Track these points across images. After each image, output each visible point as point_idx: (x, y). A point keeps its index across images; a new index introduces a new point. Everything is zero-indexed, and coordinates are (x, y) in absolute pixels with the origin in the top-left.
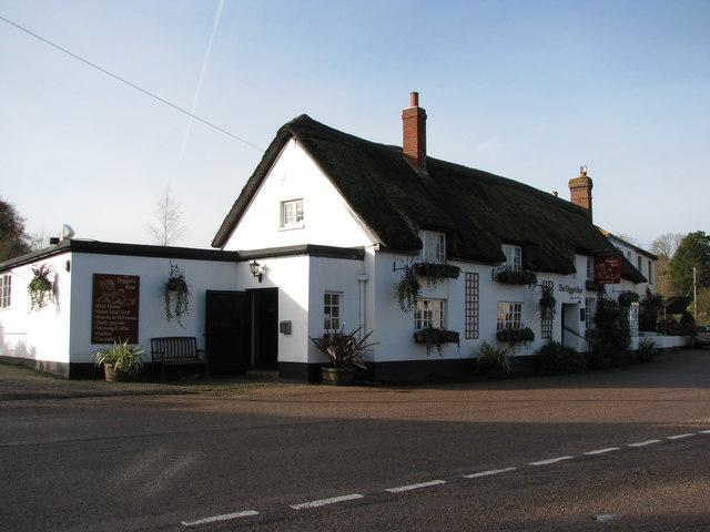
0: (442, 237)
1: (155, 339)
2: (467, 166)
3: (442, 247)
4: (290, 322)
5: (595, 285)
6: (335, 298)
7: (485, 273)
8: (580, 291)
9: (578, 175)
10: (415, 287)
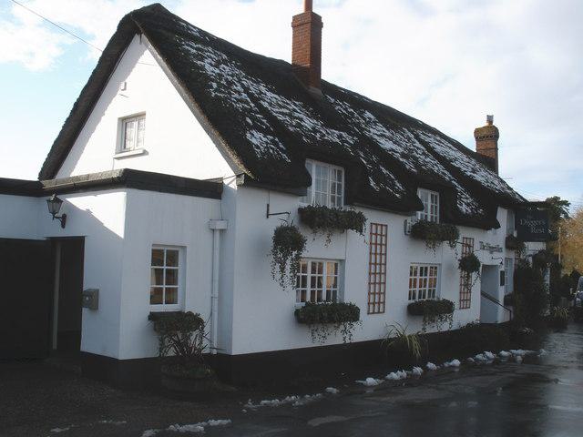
0: (340, 172)
2: (48, 151)
3: (339, 186)
4: (97, 291)
5: (513, 244)
6: (173, 257)
7: (395, 226)
8: (499, 250)
9: (484, 123)
10: (299, 244)
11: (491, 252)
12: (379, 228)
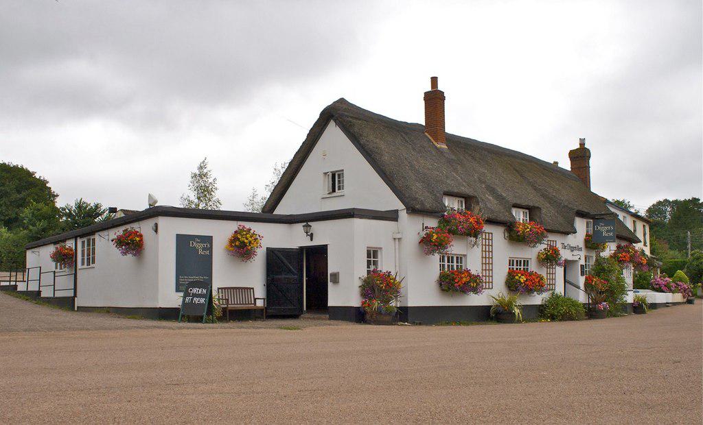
1: (222, 288)
8: (580, 249)
11: (572, 251)
12: (487, 287)
